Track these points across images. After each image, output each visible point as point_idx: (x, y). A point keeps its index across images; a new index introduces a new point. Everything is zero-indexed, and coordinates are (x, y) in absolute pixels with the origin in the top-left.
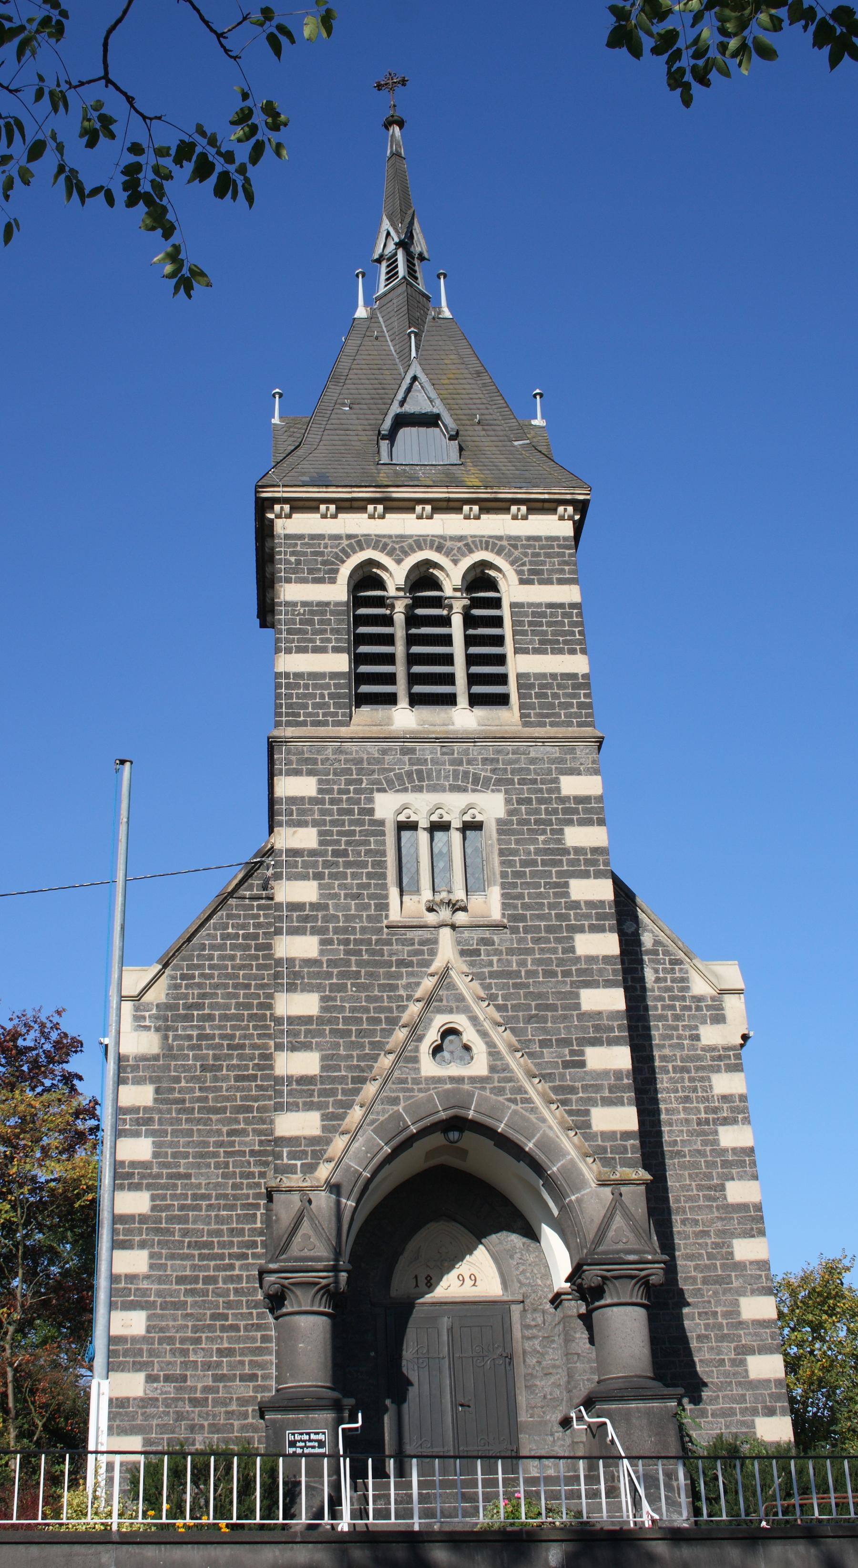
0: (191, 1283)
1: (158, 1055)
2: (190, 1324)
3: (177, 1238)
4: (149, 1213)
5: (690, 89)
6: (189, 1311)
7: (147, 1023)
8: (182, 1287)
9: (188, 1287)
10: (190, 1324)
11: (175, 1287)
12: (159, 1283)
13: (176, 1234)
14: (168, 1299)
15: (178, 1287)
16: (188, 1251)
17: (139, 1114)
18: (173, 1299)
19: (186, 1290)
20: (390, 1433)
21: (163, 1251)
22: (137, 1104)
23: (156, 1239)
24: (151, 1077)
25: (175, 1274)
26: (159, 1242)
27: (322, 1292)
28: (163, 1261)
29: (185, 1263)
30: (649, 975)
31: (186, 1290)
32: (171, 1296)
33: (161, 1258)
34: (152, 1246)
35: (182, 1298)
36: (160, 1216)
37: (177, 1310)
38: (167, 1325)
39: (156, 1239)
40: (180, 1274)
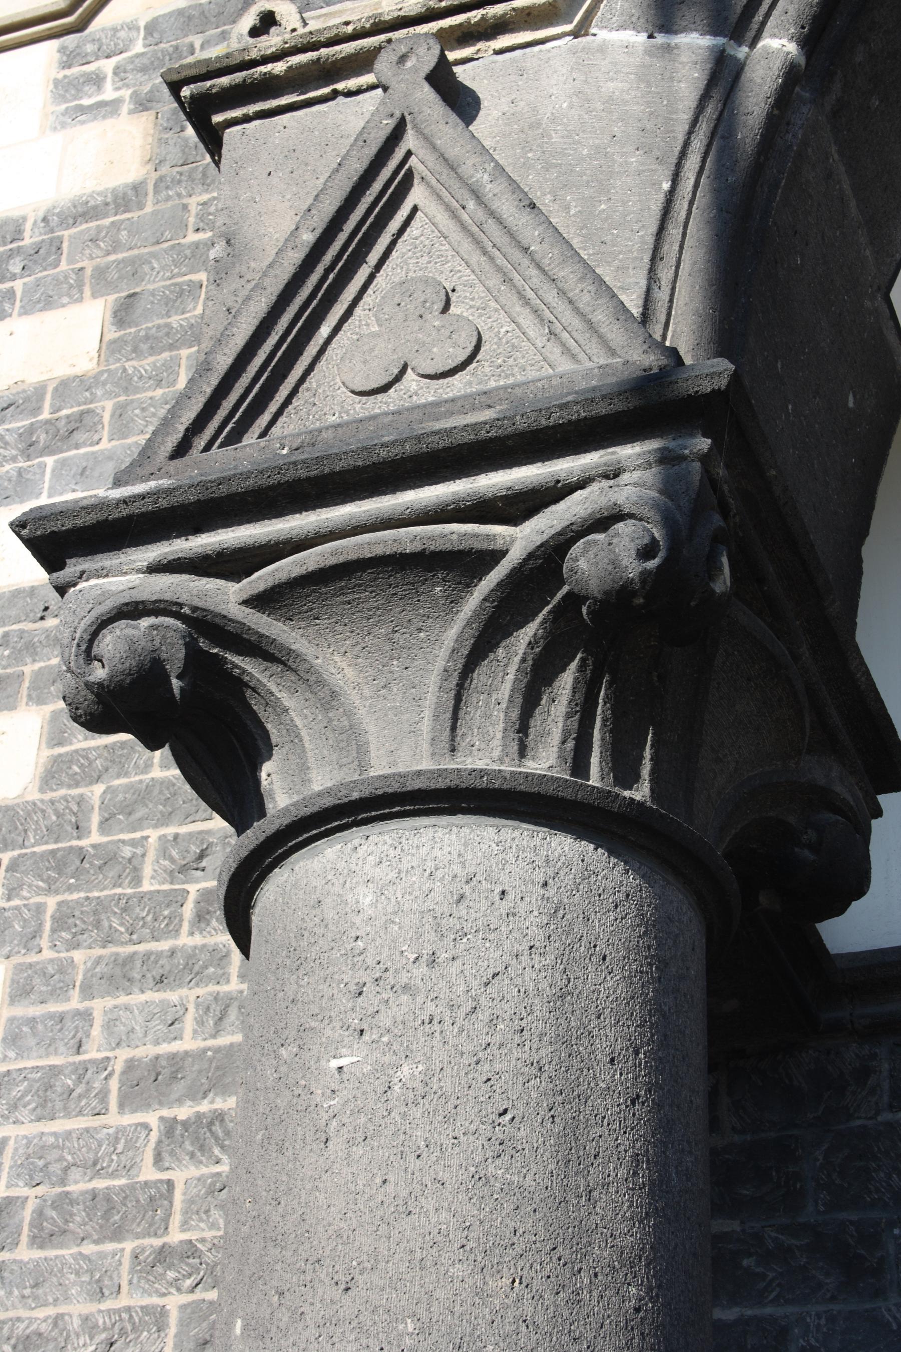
0: (197, 1093)
1: (138, 188)
2: (174, 1302)
3: (147, 886)
4: (34, 795)
5: (153, 828)
6: (175, 1236)
7: (109, 93)
8: (152, 1118)
9: (183, 1112)
10: (174, 1302)
11: (116, 1119)
12: (44, 1113)
13: (148, 870)
14: (78, 1186)
15: (129, 1119)
16: (198, 940)
17: (37, 410)
18: (100, 1184)
19: (170, 1126)
20: (27, 35)
21: (78, 956)
22: (33, 377)
23: (51, 902)
24: (100, 273)
25: (123, 1055)
26: (61, 921)
27: (567, 680)
28: (75, 1003)
29: (173, 996)
30: (678, 284)
31: (170, 1126)
32: (95, 1168)
33: (60, 991)
34: (30, 940)
35: (148, 1173)
36: (81, 801)
37: (117, 1234)
38: (57, 1320)
39: (51, 902)
40: (146, 1051)
